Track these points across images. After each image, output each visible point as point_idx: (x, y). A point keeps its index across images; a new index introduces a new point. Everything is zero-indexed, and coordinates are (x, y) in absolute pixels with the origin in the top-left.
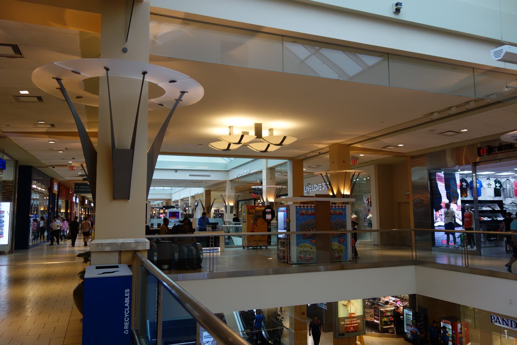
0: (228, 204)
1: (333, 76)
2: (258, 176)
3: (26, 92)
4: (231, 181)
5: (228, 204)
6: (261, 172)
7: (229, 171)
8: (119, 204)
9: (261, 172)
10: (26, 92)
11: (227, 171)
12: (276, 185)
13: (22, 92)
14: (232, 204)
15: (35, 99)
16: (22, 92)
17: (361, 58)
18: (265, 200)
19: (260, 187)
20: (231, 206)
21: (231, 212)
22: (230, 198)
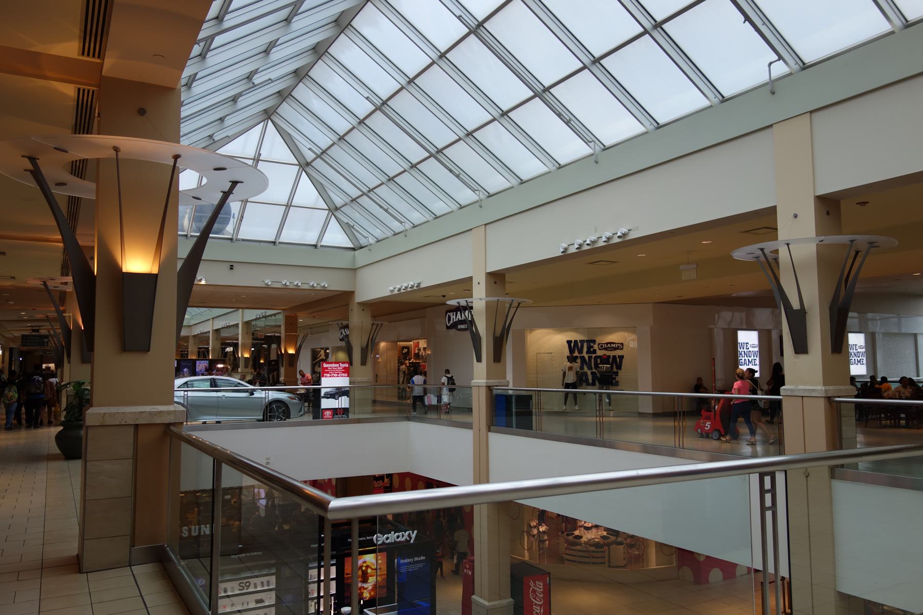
0: (286, 351)
4: (194, 336)
5: (286, 351)
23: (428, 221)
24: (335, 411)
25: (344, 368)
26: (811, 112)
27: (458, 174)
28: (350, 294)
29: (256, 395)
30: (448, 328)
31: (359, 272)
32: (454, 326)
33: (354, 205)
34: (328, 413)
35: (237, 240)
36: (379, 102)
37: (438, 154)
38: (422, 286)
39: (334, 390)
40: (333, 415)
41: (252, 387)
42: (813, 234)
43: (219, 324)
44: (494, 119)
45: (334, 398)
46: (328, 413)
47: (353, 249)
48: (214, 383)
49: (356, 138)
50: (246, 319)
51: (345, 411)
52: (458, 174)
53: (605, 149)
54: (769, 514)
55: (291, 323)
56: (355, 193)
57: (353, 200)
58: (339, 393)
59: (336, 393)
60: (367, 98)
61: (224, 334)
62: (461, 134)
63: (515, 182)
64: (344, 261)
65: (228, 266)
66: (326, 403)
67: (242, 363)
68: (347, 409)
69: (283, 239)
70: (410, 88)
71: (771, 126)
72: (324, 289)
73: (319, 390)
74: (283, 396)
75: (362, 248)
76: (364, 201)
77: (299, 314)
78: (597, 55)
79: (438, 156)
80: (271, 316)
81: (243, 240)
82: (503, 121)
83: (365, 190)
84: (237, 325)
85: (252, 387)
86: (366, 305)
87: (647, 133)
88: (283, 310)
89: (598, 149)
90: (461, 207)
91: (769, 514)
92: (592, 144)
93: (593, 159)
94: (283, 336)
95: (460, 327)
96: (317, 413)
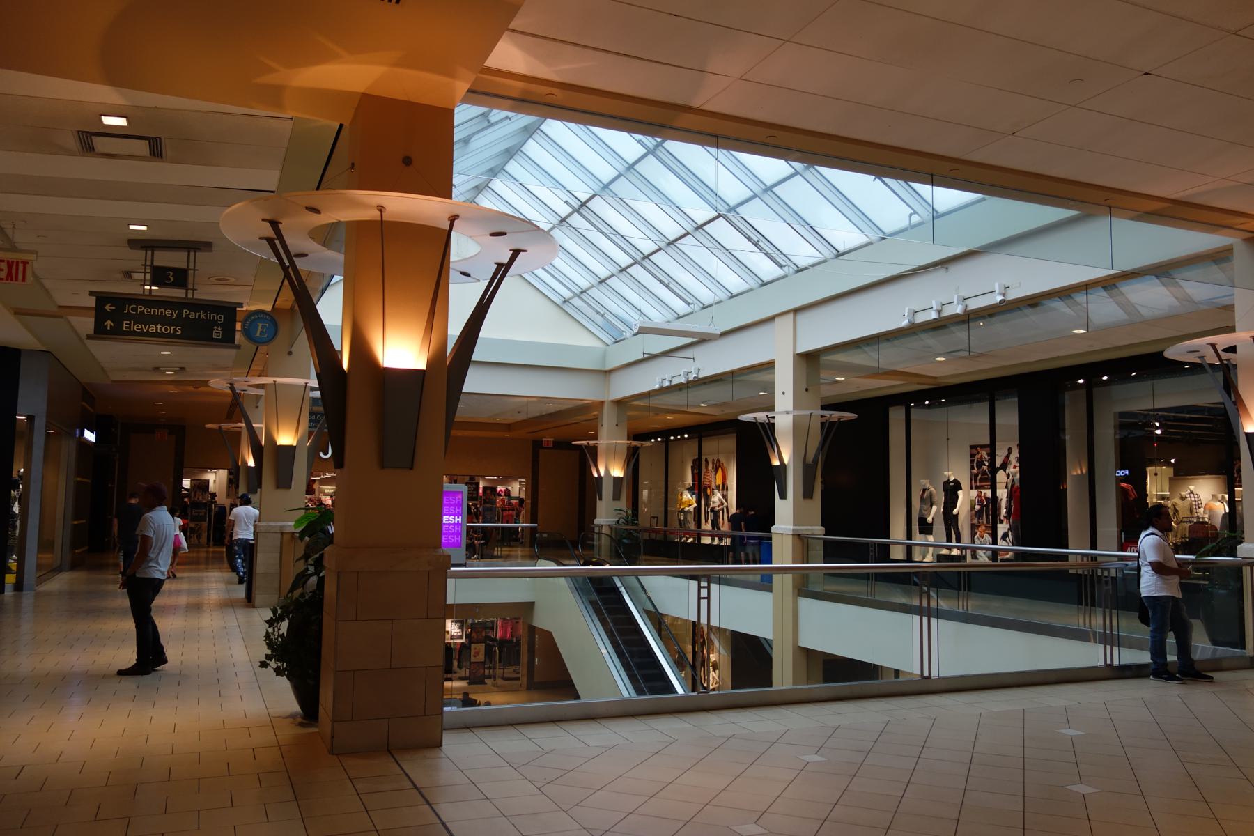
0: (607, 471)
1: (912, 184)
2: (762, 377)
3: (121, 122)
4: (619, 403)
5: (607, 471)
6: (769, 366)
7: (610, 371)
8: (281, 492)
9: (769, 366)
10: (121, 122)
11: (606, 372)
12: (823, 408)
13: (107, 121)
14: (617, 472)
15: (142, 147)
16: (107, 121)
17: (882, 201)
18: (602, 473)
19: (592, 443)
20: (615, 478)
21: (616, 497)
22: (612, 452)
23: (751, 290)
26: (796, 311)
27: (758, 241)
33: (623, 276)
36: (576, 204)
37: (727, 213)
42: (791, 408)
44: (755, 196)
49: (597, 205)
52: (758, 241)
54: (704, 603)
56: (624, 260)
57: (623, 270)
60: (566, 202)
62: (757, 190)
63: (828, 253)
67: (607, 490)
70: (629, 175)
71: (771, 319)
76: (636, 271)
78: (769, 183)
79: (644, 263)
82: (766, 198)
83: (638, 257)
87: (870, 244)
90: (839, 254)
91: (704, 603)
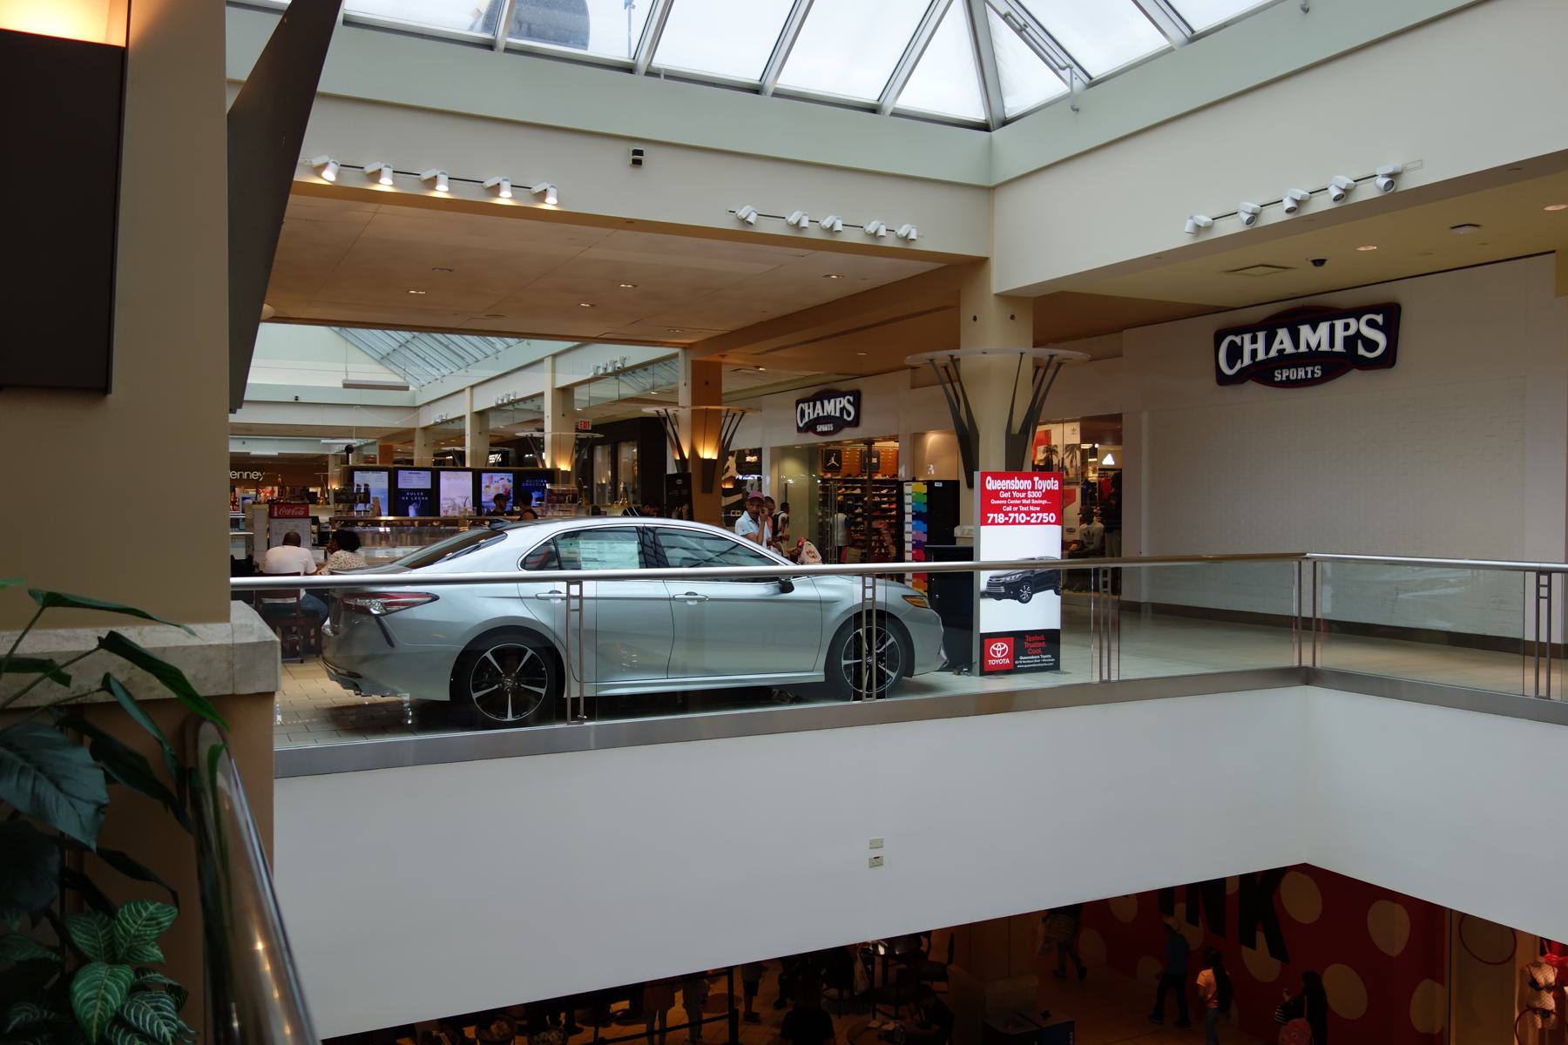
4: (425, 429)
24: (1019, 639)
25: (1048, 494)
28: (975, 266)
29: (801, 590)
30: (1222, 380)
31: (1009, 203)
32: (1262, 373)
34: (999, 648)
35: (652, 73)
38: (1408, 183)
39: (1015, 575)
40: (1015, 654)
41: (792, 567)
43: (487, 399)
45: (1016, 596)
46: (999, 648)
47: (984, 127)
48: (652, 553)
50: (561, 383)
51: (1049, 639)
53: (1093, 83)
55: (706, 383)
58: (1024, 581)
59: (1024, 581)
61: (497, 424)
64: (959, 160)
65: (624, 152)
66: (995, 616)
68: (1057, 631)
69: (789, 79)
72: (905, 252)
73: (968, 578)
74: (886, 594)
75: (1005, 122)
77: (733, 358)
80: (644, 366)
81: (672, 76)
84: (462, 418)
85: (792, 567)
86: (1011, 299)
88: (686, 348)
89: (1078, 84)
92: (1066, 74)
93: (1070, 105)
94: (548, 437)
95: (820, 428)
96: (963, 645)
